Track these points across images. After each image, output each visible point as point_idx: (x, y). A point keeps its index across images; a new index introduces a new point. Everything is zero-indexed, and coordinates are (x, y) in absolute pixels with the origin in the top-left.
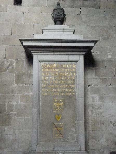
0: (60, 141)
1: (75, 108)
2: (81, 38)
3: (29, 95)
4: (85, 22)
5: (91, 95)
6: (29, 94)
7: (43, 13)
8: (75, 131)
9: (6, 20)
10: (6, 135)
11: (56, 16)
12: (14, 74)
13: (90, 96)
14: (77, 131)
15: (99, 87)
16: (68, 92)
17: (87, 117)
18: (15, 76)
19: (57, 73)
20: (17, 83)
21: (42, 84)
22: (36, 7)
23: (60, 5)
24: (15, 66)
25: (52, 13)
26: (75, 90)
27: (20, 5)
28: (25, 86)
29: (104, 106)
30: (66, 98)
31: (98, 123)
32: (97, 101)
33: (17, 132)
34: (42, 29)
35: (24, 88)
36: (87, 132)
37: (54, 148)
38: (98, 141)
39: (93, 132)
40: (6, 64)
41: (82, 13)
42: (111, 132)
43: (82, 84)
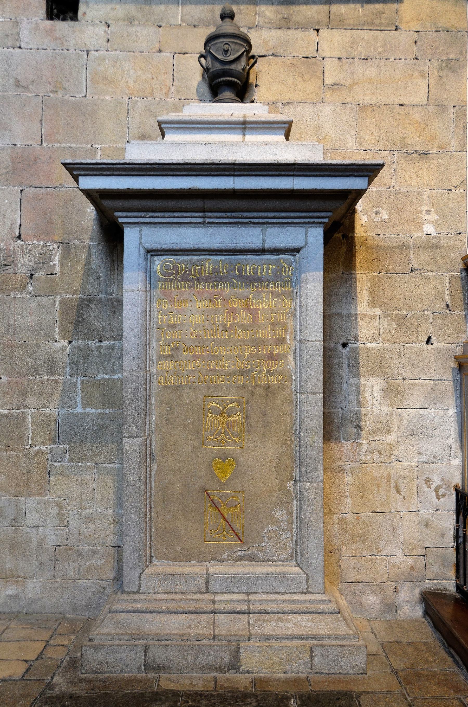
0: (228, 555)
2: (317, 158)
3: (113, 380)
4: (336, 85)
6: (115, 377)
7: (167, 55)
8: (288, 521)
9: (18, 84)
10: (34, 530)
11: (218, 66)
12: (55, 302)
15: (384, 350)
16: (260, 372)
18: (58, 310)
21: (157, 340)
22: (139, 29)
23: (236, 18)
24: (58, 269)
27: (72, 19)
28: (99, 347)
29: (401, 420)
30: (253, 394)
31: (379, 486)
32: (377, 404)
34: (160, 118)
35: (95, 353)
37: (207, 583)
39: (358, 518)
40: (24, 263)
41: (325, 51)
42: (428, 519)
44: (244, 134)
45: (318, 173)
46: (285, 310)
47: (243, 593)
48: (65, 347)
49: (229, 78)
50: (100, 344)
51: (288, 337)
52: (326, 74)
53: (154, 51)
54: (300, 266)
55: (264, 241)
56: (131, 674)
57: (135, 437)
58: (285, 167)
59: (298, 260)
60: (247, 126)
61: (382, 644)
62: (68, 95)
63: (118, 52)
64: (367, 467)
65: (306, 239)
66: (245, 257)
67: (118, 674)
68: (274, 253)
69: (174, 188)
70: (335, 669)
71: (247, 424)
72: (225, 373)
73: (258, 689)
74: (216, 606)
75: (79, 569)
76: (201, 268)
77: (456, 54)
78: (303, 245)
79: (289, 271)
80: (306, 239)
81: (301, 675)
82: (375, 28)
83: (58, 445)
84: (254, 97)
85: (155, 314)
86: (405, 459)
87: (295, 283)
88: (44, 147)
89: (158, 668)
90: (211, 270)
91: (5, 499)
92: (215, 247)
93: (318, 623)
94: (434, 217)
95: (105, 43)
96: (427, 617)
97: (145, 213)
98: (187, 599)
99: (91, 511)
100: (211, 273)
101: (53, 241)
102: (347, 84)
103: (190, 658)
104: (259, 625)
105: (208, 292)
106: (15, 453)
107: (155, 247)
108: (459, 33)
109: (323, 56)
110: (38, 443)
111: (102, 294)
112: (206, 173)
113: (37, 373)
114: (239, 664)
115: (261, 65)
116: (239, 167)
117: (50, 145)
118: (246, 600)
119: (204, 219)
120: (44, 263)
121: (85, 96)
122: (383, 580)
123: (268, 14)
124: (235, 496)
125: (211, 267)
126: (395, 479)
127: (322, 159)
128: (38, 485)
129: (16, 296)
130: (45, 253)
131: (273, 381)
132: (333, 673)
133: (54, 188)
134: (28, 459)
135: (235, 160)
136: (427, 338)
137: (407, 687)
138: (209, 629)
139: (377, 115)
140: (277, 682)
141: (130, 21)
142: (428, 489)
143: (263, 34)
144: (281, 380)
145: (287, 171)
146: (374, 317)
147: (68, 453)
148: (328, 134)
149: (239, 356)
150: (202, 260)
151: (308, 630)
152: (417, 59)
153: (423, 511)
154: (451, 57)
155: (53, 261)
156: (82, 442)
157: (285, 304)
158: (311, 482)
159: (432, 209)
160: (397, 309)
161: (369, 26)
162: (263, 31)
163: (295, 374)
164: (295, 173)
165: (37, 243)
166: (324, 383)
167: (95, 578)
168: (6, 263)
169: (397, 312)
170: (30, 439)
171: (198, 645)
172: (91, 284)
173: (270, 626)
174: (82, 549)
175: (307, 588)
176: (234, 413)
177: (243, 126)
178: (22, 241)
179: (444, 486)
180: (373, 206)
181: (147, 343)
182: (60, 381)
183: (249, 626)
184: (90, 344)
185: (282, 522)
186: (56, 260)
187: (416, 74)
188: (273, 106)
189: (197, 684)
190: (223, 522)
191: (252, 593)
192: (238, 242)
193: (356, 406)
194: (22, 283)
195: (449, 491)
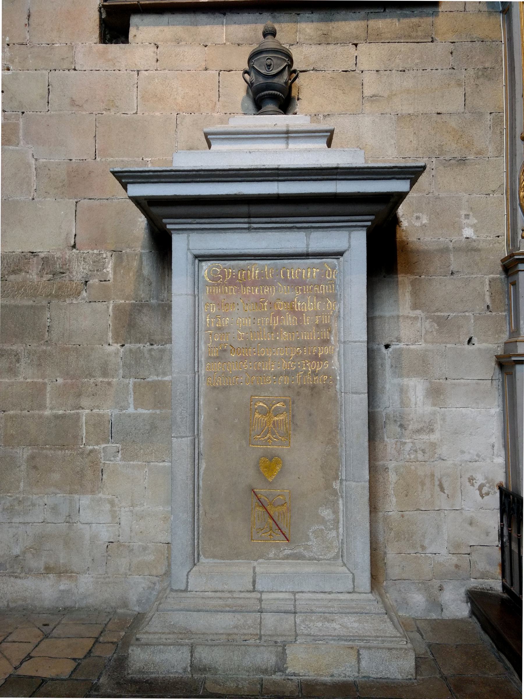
0: (275, 554)
1: (332, 433)
2: (358, 161)
3: (164, 382)
4: (374, 98)
5: (396, 381)
6: (166, 378)
8: (334, 520)
9: (73, 102)
10: (87, 526)
11: (261, 80)
12: (108, 307)
13: (389, 382)
14: (341, 518)
15: (426, 350)
16: (306, 373)
17: (381, 463)
18: (111, 314)
19: (263, 302)
20: (121, 339)
21: (205, 343)
24: (111, 276)
25: (247, 67)
26: (331, 365)
28: (150, 350)
29: (444, 420)
30: (298, 394)
31: (423, 484)
32: (420, 403)
33: (125, 518)
34: (207, 130)
35: (147, 355)
36: (380, 514)
37: (254, 582)
38: (420, 550)
39: (403, 516)
41: (364, 64)
43: (362, 342)
44: (287, 144)
45: (361, 177)
46: (329, 312)
47: (289, 592)
48: (118, 350)
49: (272, 92)
50: (151, 347)
51: (332, 338)
52: (365, 87)
53: (200, 69)
54: (344, 269)
55: (308, 245)
56: (177, 675)
57: (184, 437)
58: (328, 171)
59: (341, 264)
60: (290, 135)
61: (430, 646)
62: (120, 113)
63: (166, 71)
64: (411, 465)
65: (349, 242)
66: (289, 261)
67: (164, 676)
68: (318, 257)
69: (220, 193)
70: (383, 673)
71: (293, 423)
72: (271, 373)
73: (305, 695)
74: (263, 606)
75: (130, 565)
76: (247, 273)
77: (492, 62)
78: (346, 248)
79: (333, 274)
80: (349, 242)
81: (348, 678)
82: (411, 41)
83: (111, 445)
84: (297, 110)
85: (204, 317)
86: (448, 458)
87: (339, 285)
88: (98, 161)
89: (204, 669)
90: (256, 274)
91: (60, 496)
92: (261, 251)
93: (365, 624)
94: (473, 220)
95: (154, 63)
96: (473, 617)
97: (193, 220)
98: (234, 598)
99: (142, 508)
100: (257, 277)
101: (106, 250)
102: (386, 95)
103: (236, 659)
104: (305, 624)
105: (254, 296)
106: (70, 452)
107: (202, 252)
108: (494, 43)
109: (362, 69)
110: (91, 442)
111: (153, 299)
112: (251, 179)
113: (91, 375)
114: (285, 666)
115: (302, 81)
116: (282, 172)
117: (103, 160)
118: (292, 599)
119: (250, 225)
120: (97, 271)
121: (136, 113)
122: (428, 578)
123: (308, 31)
124: (282, 495)
125: (257, 272)
126: (439, 477)
127: (364, 162)
128: (92, 483)
129: (71, 302)
130: (98, 262)
131: (318, 381)
132: (381, 678)
133: (107, 199)
134: (82, 458)
135: (279, 165)
136: (468, 339)
137: (458, 695)
138: (255, 628)
139: (415, 124)
140: (325, 687)
141: (178, 41)
142: (472, 487)
143: (304, 50)
144: (326, 380)
145: (330, 175)
146: (416, 318)
147: (120, 452)
148: (368, 144)
149: (285, 357)
150: (248, 265)
151: (354, 631)
152: (453, 69)
153: (467, 509)
154: (487, 65)
155: (106, 268)
156: (134, 441)
157: (329, 306)
158: (357, 482)
159: (471, 213)
160: (438, 310)
161: (406, 39)
162: (304, 47)
163: (340, 374)
164: (338, 177)
165: (91, 252)
166: (368, 383)
167: (146, 574)
168: (62, 271)
169: (439, 314)
170: (84, 439)
171: (244, 645)
172: (143, 290)
173: (317, 626)
174: (133, 546)
175: (354, 588)
176: (280, 412)
177: (286, 136)
178: (77, 249)
179: (487, 485)
180: (413, 211)
181: (196, 346)
182: (112, 383)
183: (295, 626)
184: (142, 348)
185: (328, 521)
186: (109, 268)
187: (453, 82)
188: (315, 118)
189: (243, 687)
190: (271, 521)
191: (298, 592)
192: (283, 246)
193: (399, 406)
194: (77, 290)
195: (492, 489)
